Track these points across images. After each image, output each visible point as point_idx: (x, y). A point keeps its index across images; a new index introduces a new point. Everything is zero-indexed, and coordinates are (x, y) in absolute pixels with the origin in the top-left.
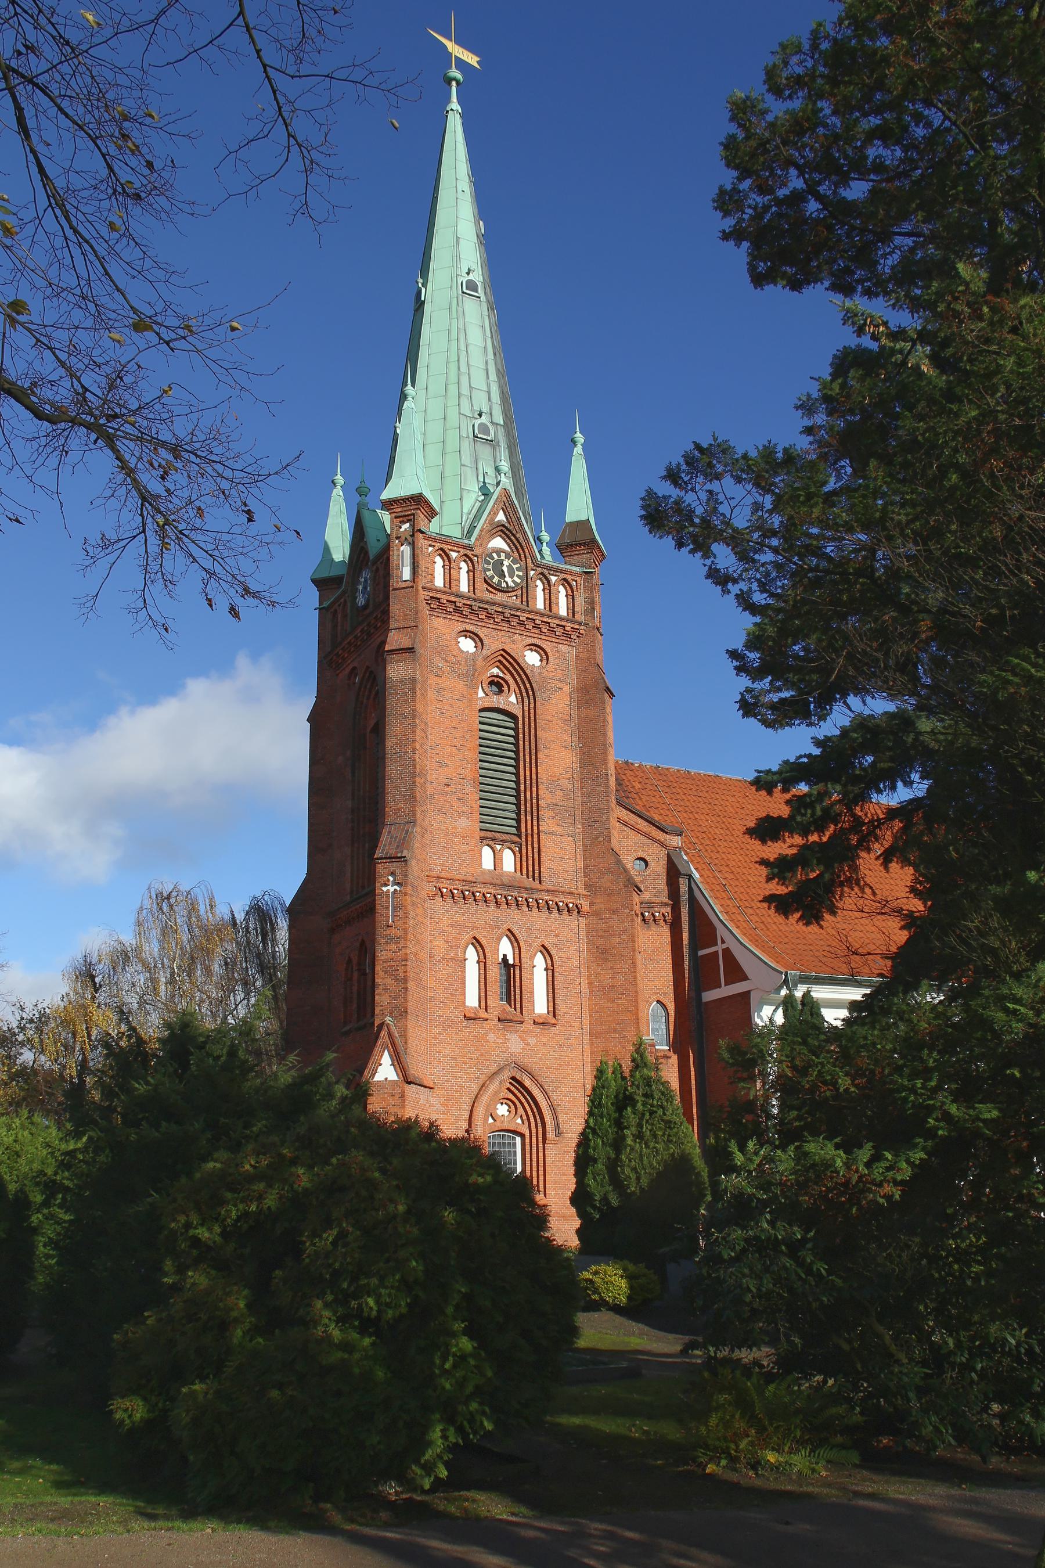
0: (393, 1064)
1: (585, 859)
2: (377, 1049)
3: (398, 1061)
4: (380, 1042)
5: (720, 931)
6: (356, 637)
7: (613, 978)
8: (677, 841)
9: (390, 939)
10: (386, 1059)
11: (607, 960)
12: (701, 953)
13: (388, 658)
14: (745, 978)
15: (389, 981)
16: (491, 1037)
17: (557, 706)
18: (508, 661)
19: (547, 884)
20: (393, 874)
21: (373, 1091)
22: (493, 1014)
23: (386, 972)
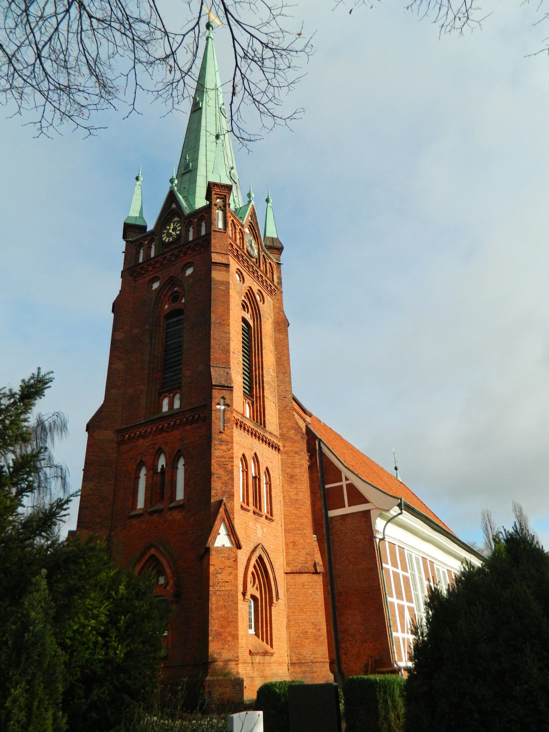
0: (228, 535)
1: (279, 418)
2: (217, 522)
3: (232, 533)
4: (219, 516)
5: (345, 472)
6: (164, 258)
7: (297, 494)
8: (308, 419)
10: (222, 530)
11: (293, 482)
12: (327, 486)
13: (213, 267)
14: (366, 501)
15: (221, 472)
16: (251, 524)
20: (223, 398)
21: (213, 554)
23: (219, 465)
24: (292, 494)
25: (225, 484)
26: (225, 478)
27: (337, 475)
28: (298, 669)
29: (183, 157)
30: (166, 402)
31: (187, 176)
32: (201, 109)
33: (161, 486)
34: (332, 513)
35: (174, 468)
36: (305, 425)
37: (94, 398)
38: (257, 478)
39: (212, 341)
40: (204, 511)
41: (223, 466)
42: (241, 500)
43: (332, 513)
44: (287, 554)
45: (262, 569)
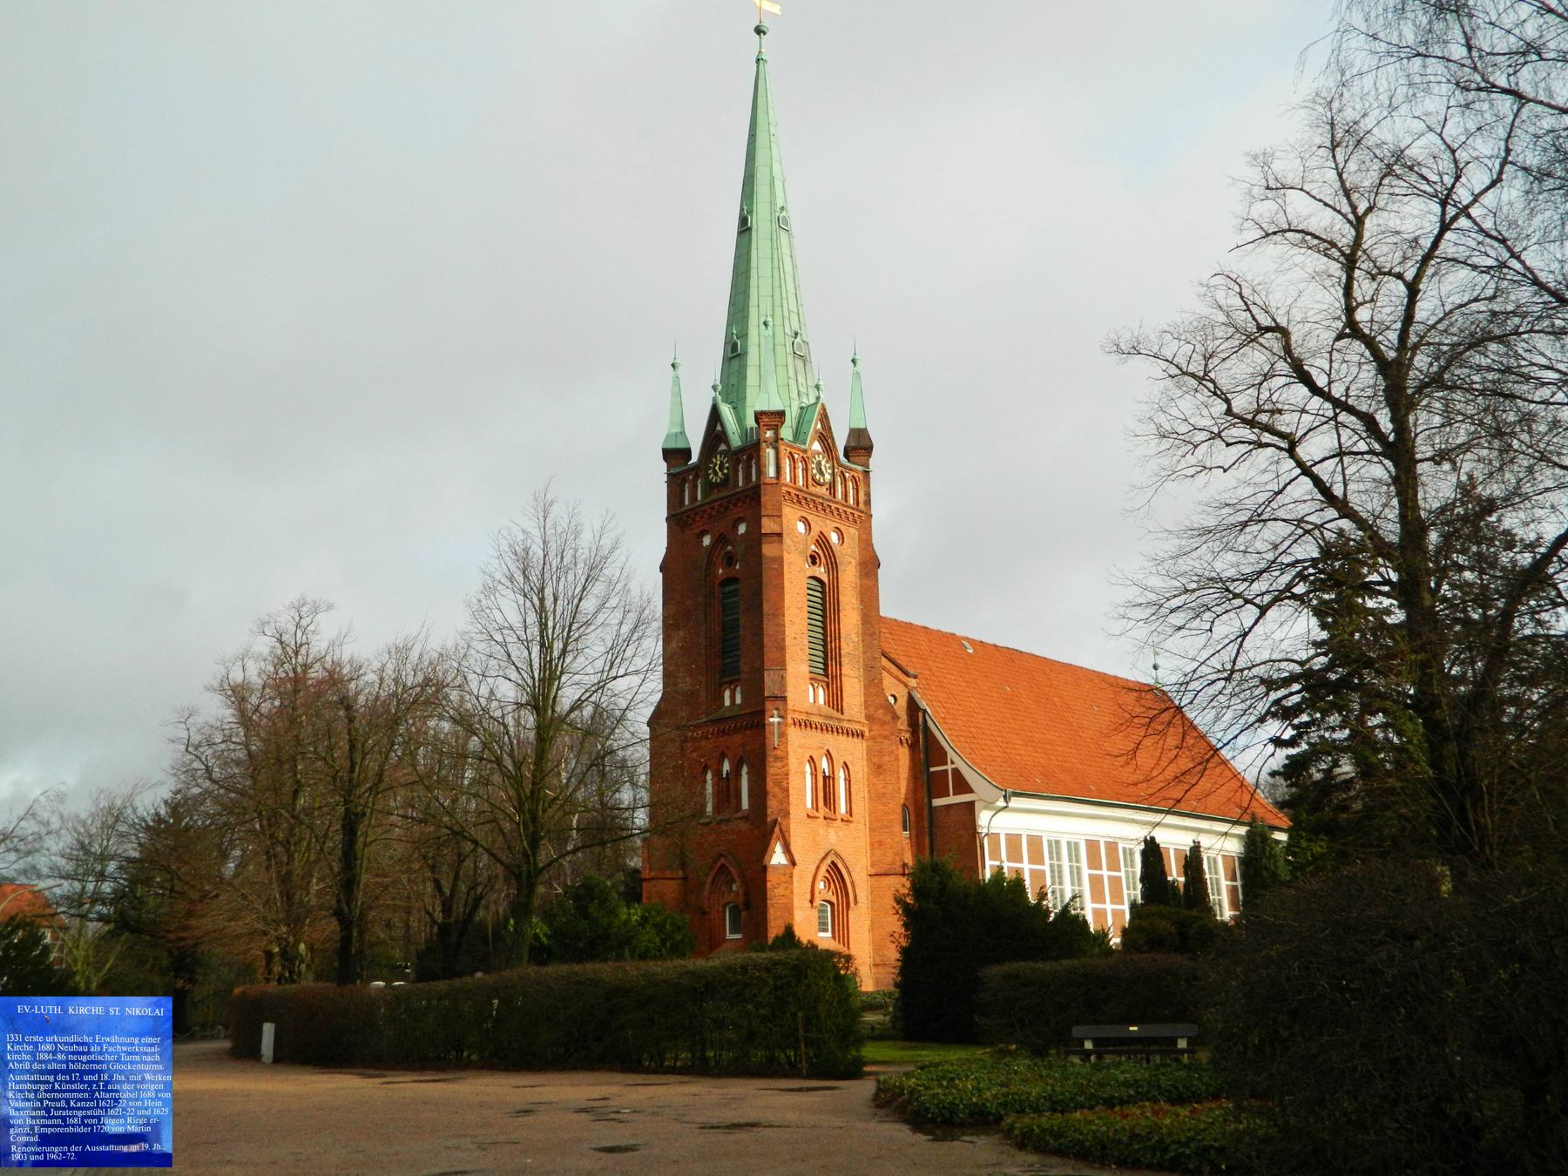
3: (787, 850)
5: (951, 754)
8: (913, 682)
9: (776, 758)
10: (778, 848)
14: (971, 791)
15: (776, 790)
17: (849, 576)
18: (823, 541)
19: (846, 716)
22: (821, 814)
24: (879, 785)
25: (781, 802)
26: (781, 796)
27: (942, 758)
28: (881, 970)
29: (729, 335)
30: (727, 694)
31: (735, 363)
32: (750, 229)
33: (726, 792)
34: (937, 802)
35: (739, 775)
36: (905, 691)
37: (653, 689)
38: (829, 780)
39: (766, 640)
40: (762, 827)
41: (778, 784)
42: (809, 805)
43: (937, 802)
44: (872, 855)
45: (836, 875)
